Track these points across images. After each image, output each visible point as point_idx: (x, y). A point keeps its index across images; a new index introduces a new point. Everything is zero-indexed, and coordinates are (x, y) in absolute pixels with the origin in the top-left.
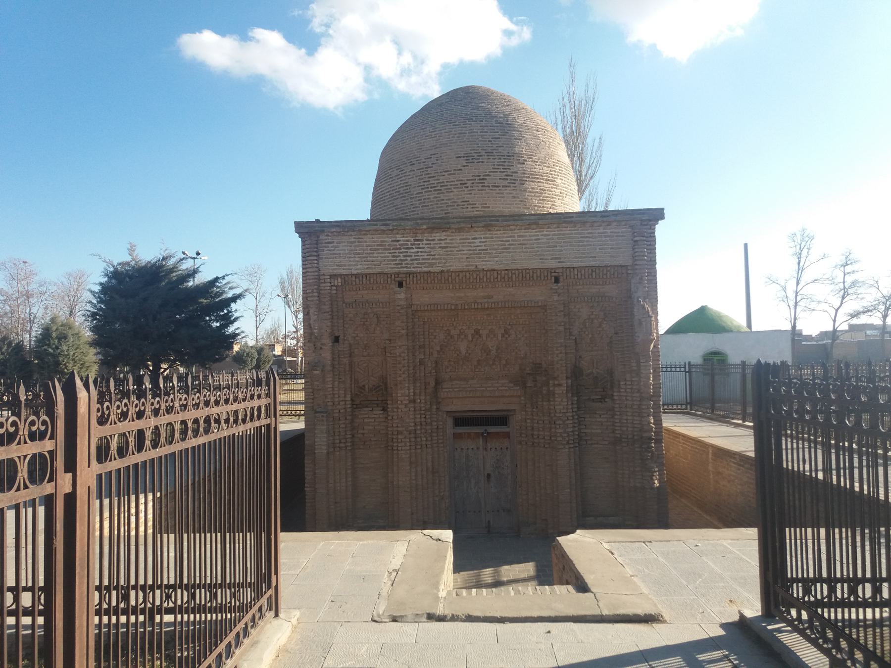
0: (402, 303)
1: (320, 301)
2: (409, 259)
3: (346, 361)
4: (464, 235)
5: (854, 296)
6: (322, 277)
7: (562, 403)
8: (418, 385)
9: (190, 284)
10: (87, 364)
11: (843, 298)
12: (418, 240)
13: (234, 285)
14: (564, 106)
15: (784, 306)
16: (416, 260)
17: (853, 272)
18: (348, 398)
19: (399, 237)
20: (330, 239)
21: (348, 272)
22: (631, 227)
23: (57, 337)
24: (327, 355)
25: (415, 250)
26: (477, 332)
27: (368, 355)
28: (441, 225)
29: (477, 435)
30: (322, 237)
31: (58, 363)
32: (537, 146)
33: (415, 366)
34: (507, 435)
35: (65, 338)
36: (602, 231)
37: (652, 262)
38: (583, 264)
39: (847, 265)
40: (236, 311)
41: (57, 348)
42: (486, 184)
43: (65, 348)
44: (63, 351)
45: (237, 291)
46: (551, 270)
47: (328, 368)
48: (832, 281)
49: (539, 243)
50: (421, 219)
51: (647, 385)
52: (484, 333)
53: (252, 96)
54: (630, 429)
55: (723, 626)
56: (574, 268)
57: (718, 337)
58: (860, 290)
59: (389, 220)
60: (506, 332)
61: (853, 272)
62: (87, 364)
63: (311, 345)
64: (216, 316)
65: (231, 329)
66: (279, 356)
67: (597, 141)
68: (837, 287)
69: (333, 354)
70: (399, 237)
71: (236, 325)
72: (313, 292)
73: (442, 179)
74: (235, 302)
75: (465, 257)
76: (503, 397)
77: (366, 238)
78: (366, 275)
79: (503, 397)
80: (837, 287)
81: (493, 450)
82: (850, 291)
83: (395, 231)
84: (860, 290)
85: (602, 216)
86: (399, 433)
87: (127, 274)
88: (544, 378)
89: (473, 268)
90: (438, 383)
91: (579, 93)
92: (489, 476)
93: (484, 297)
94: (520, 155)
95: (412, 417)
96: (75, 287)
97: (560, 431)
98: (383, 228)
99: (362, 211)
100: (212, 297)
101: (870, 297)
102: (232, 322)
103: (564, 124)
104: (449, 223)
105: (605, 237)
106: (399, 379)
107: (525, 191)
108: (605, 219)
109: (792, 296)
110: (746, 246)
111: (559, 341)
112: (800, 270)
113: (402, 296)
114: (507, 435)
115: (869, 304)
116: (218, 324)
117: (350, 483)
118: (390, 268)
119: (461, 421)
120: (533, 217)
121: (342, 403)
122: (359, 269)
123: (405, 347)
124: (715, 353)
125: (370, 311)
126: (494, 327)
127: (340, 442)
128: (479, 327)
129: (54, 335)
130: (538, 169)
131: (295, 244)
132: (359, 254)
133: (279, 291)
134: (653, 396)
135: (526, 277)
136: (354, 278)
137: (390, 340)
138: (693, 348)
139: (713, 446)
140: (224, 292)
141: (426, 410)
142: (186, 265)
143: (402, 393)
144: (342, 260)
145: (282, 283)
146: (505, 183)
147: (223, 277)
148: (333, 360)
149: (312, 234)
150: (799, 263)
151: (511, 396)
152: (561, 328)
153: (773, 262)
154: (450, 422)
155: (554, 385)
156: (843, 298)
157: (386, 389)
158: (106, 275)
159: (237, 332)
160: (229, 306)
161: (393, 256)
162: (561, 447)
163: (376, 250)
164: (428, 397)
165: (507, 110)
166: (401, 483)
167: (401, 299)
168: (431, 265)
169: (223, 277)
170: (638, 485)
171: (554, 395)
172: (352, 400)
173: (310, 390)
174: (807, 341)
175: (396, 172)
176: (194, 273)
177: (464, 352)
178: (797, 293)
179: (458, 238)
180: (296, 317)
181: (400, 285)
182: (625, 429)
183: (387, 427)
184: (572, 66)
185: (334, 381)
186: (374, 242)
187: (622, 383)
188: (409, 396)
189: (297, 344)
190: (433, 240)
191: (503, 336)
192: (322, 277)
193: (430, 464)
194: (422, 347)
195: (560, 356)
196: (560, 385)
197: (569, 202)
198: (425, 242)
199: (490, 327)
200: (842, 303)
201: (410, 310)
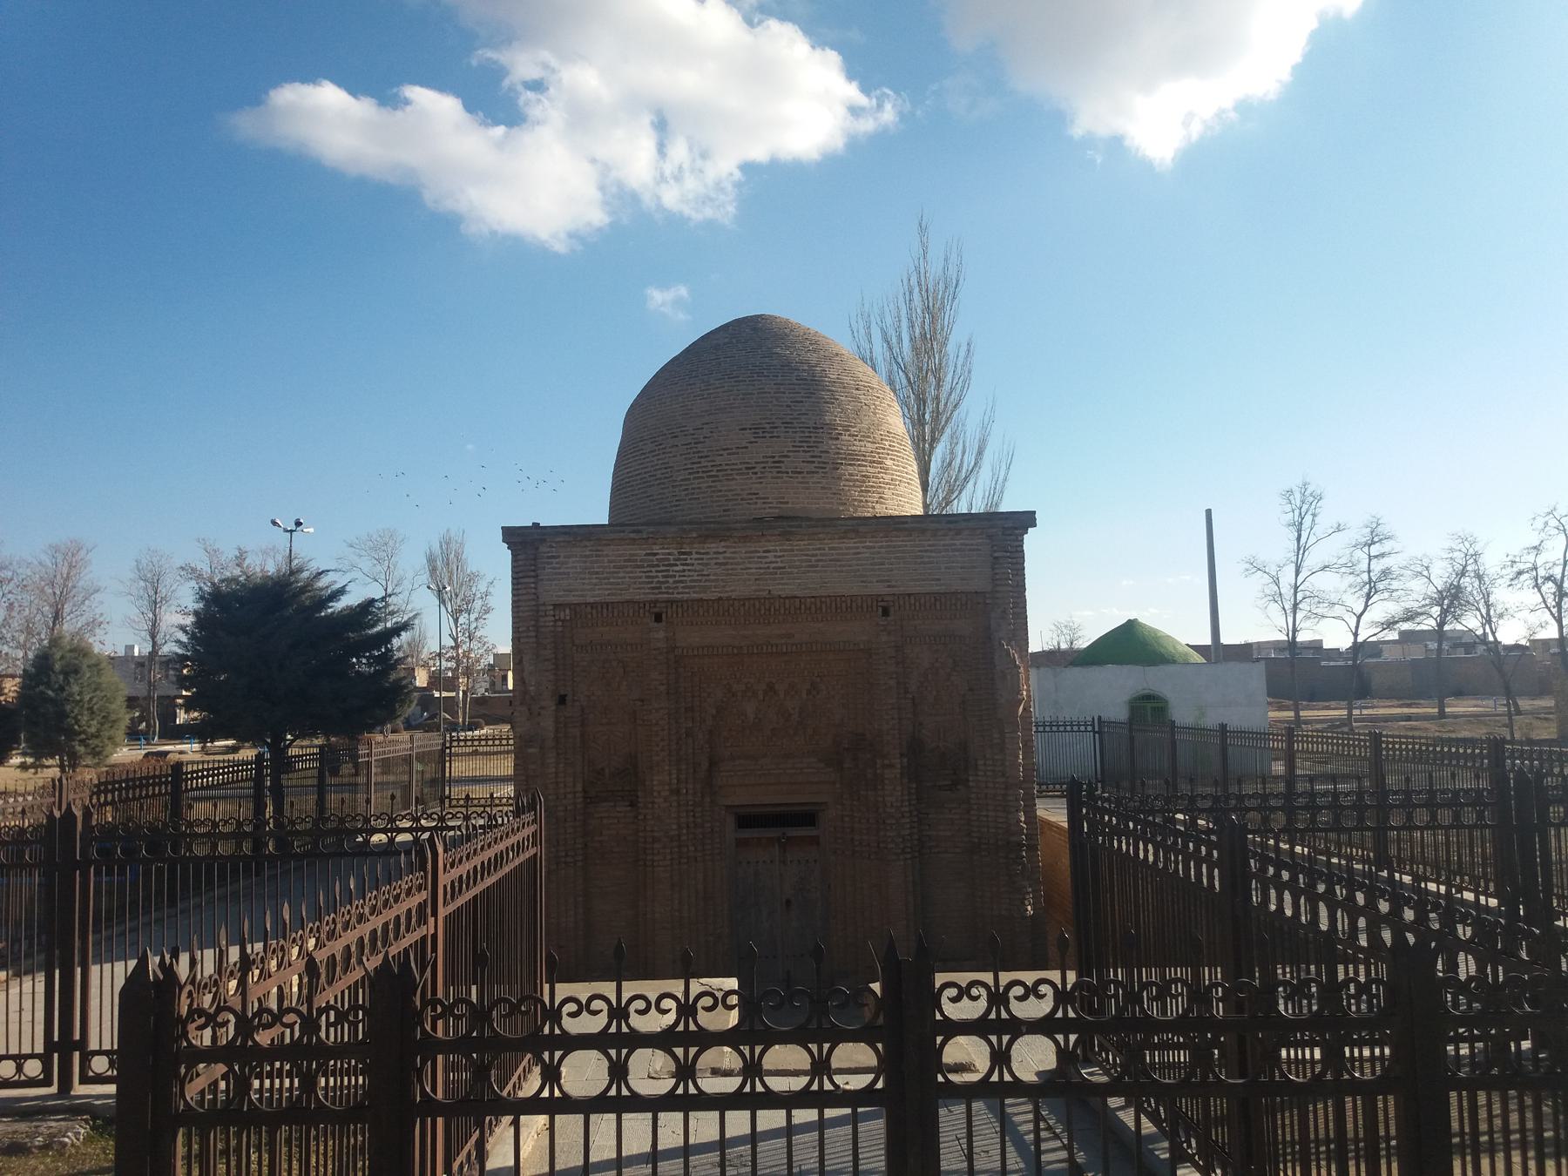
5: (1386, 595)
10: (113, 717)
11: (1369, 597)
14: (911, 293)
15: (1275, 609)
17: (1382, 555)
18: (579, 788)
19: (656, 549)
21: (581, 600)
22: (990, 537)
23: (62, 672)
24: (548, 723)
28: (715, 530)
30: (543, 549)
31: (63, 715)
34: (815, 841)
35: (76, 671)
38: (922, 590)
39: (1373, 543)
41: (62, 689)
43: (76, 689)
44: (71, 695)
46: (878, 598)
48: (1351, 568)
50: (690, 523)
51: (1015, 765)
55: (1038, 1074)
57: (1152, 672)
58: (1395, 585)
61: (1382, 555)
62: (113, 717)
64: (368, 658)
67: (964, 348)
68: (1359, 580)
70: (656, 549)
73: (718, 460)
80: (1359, 580)
82: (1380, 586)
84: (1395, 585)
87: (233, 595)
89: (765, 594)
91: (935, 269)
94: (832, 426)
96: (65, 571)
99: (599, 515)
101: (1416, 591)
103: (910, 320)
104: (729, 529)
109: (1287, 591)
110: (1209, 512)
112: (1301, 550)
113: (661, 635)
114: (815, 841)
115: (1416, 605)
119: (747, 820)
124: (1149, 697)
129: (57, 667)
130: (858, 446)
133: (425, 577)
135: (841, 606)
138: (1109, 695)
144: (573, 583)
145: (431, 560)
146: (811, 467)
148: (557, 731)
149: (526, 544)
150: (1299, 539)
152: (892, 683)
153: (1258, 535)
154: (731, 821)
156: (1369, 597)
158: (202, 598)
160: (389, 641)
165: (813, 358)
172: (584, 791)
174: (1329, 660)
176: (341, 591)
178: (1296, 588)
180: (456, 621)
181: (658, 618)
184: (923, 229)
187: (981, 762)
191: (809, 692)
196: (891, 766)
197: (907, 501)
200: (1366, 606)
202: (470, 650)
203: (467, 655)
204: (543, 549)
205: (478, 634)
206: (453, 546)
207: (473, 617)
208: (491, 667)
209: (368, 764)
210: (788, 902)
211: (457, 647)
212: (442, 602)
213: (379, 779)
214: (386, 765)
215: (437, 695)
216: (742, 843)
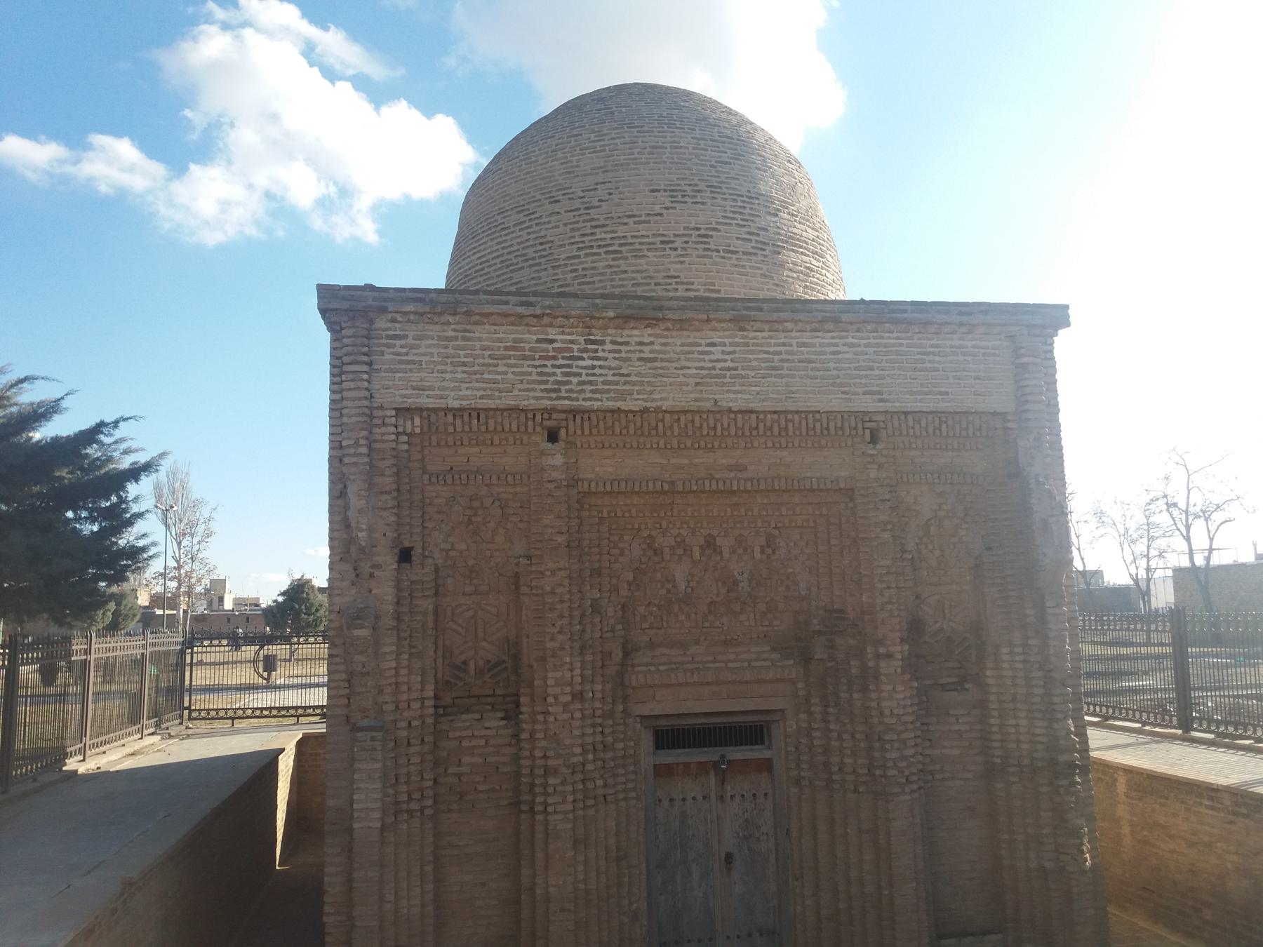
0: (556, 475)
1: (371, 465)
2: (575, 380)
3: (427, 604)
4: (692, 337)
6: (377, 413)
9: (37, 436)
12: (594, 342)
18: (429, 693)
19: (552, 333)
20: (398, 329)
22: (1011, 337)
24: (385, 590)
25: (589, 363)
26: (710, 543)
27: (475, 593)
29: (704, 768)
32: (793, 188)
33: (583, 615)
36: (957, 343)
38: (925, 407)
40: (136, 499)
42: (712, 246)
45: (142, 458)
46: (865, 417)
49: (839, 361)
53: (117, 213)
54: (1024, 746)
56: (906, 413)
59: (535, 294)
63: (346, 567)
64: (91, 511)
65: (126, 539)
66: (145, 607)
69: (399, 589)
70: (552, 333)
71: (139, 527)
72: (357, 444)
75: (692, 381)
77: (479, 332)
78: (478, 412)
81: (738, 798)
83: (546, 320)
85: (962, 314)
86: (547, 771)
88: (852, 642)
90: (628, 651)
93: (729, 468)
94: (770, 200)
97: (894, 755)
98: (520, 310)
100: (82, 469)
102: (130, 522)
104: (661, 308)
106: (550, 645)
107: (782, 266)
108: (965, 319)
111: (883, 563)
113: (558, 460)
114: (766, 766)
116: (95, 528)
118: (534, 399)
119: (670, 736)
120: (828, 307)
121: (416, 705)
123: (563, 573)
125: (484, 491)
127: (410, 798)
128: (715, 533)
131: (315, 342)
132: (464, 364)
134: (1070, 676)
136: (450, 418)
137: (529, 558)
139: (1129, 771)
140: (110, 459)
144: (434, 375)
147: (116, 424)
148: (398, 603)
152: (886, 536)
154: (647, 740)
155: (878, 656)
157: (516, 670)
159: (141, 543)
160: (123, 488)
164: (609, 686)
166: (552, 890)
168: (623, 395)
169: (116, 424)
171: (877, 678)
172: (436, 697)
177: (682, 585)
179: (677, 341)
180: (179, 544)
181: (553, 437)
182: (1013, 746)
183: (517, 758)
185: (399, 654)
186: (499, 340)
187: (1005, 650)
190: (627, 343)
193: (612, 841)
194: (597, 572)
195: (887, 594)
196: (889, 656)
198: (609, 347)
203: (189, 575)
204: (382, 323)
207: (196, 540)
211: (179, 568)
212: (167, 526)
213: (100, 688)
214: (108, 670)
215: (159, 612)
216: (662, 772)
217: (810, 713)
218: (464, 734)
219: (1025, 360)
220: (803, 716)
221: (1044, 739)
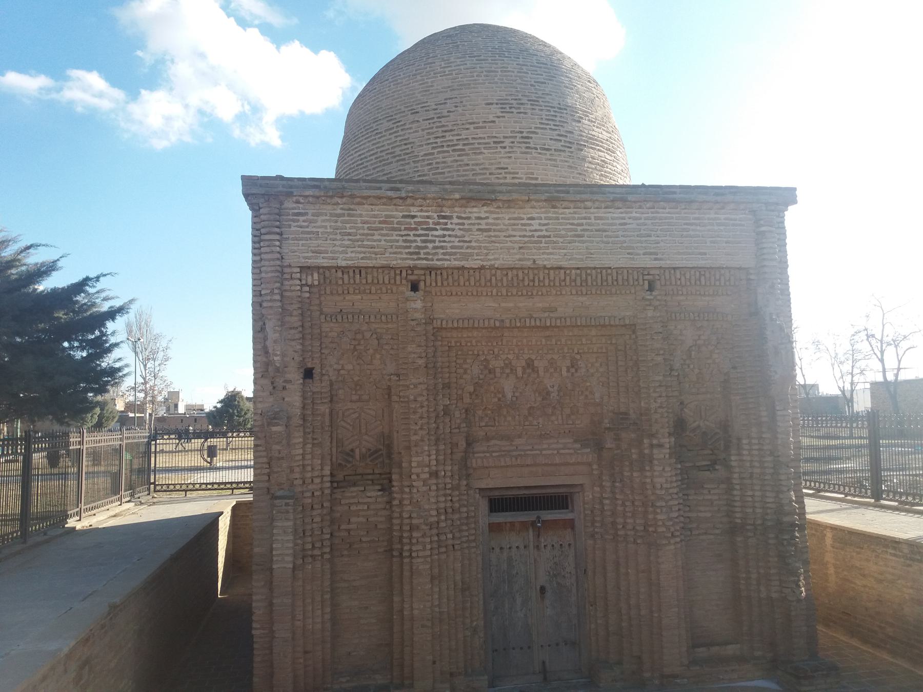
0: (418, 315)
1: (282, 307)
2: (430, 245)
3: (324, 409)
6: (286, 270)
7: (663, 475)
8: (442, 447)
12: (444, 217)
13: (111, 294)
16: (442, 247)
18: (327, 471)
19: (414, 211)
20: (301, 208)
22: (753, 212)
24: (294, 399)
25: (440, 233)
26: (530, 364)
27: (360, 400)
29: (525, 526)
30: (289, 204)
32: (592, 101)
33: (437, 417)
36: (712, 216)
37: (783, 264)
42: (532, 145)
45: (117, 303)
46: (644, 271)
47: (297, 421)
49: (625, 230)
52: (540, 364)
54: (758, 510)
56: (674, 269)
59: (401, 182)
60: (573, 365)
63: (266, 382)
64: (81, 341)
65: (107, 362)
66: (122, 412)
69: (304, 398)
70: (414, 211)
71: (116, 353)
72: (272, 293)
74: (113, 319)
75: (516, 246)
76: (567, 464)
77: (360, 210)
78: (360, 269)
79: (567, 464)
83: (409, 201)
89: (529, 263)
92: (543, 589)
93: (544, 310)
94: (574, 110)
95: (433, 500)
98: (390, 193)
100: (74, 311)
102: (109, 350)
104: (494, 192)
105: (719, 224)
108: (719, 198)
111: (657, 378)
113: (419, 305)
114: (570, 524)
116: (85, 354)
117: (327, 617)
118: (401, 260)
120: (618, 190)
121: (317, 481)
122: (351, 259)
123: (423, 387)
125: (365, 328)
126: (556, 357)
127: (313, 547)
128: (533, 357)
130: (596, 132)
131: (242, 216)
132: (350, 234)
134: (792, 460)
136: (340, 274)
137: (398, 375)
139: (834, 528)
140: (94, 305)
141: (452, 489)
142: (34, 259)
143: (420, 461)
144: (329, 242)
147: (97, 278)
148: (303, 408)
151: (578, 464)
154: (484, 506)
155: (652, 446)
157: (389, 455)
159: (117, 365)
160: (104, 325)
161: (405, 241)
162: (664, 542)
163: (376, 229)
164: (456, 468)
166: (416, 612)
167: (416, 310)
168: (466, 257)
169: (97, 278)
170: (774, 595)
171: (651, 462)
172: (332, 475)
173: (266, 464)
175: (386, 125)
179: (506, 216)
180: (145, 366)
181: (415, 287)
182: (750, 510)
183: (390, 518)
185: (305, 444)
186: (375, 216)
187: (744, 441)
188: (429, 466)
189: (145, 398)
190: (469, 218)
192: (286, 270)
193: (458, 578)
194: (447, 386)
196: (660, 446)
198: (455, 221)
199: (549, 357)
201: (430, 328)
202: (155, 385)
204: (289, 204)
205: (160, 374)
206: (144, 317)
208: (166, 400)
209: (79, 452)
210: (543, 589)
211: (145, 383)
213: (91, 469)
214: (96, 456)
215: (131, 415)
216: (495, 528)
217: (602, 486)
218: (352, 501)
219: (763, 229)
220: (597, 489)
221: (773, 506)
